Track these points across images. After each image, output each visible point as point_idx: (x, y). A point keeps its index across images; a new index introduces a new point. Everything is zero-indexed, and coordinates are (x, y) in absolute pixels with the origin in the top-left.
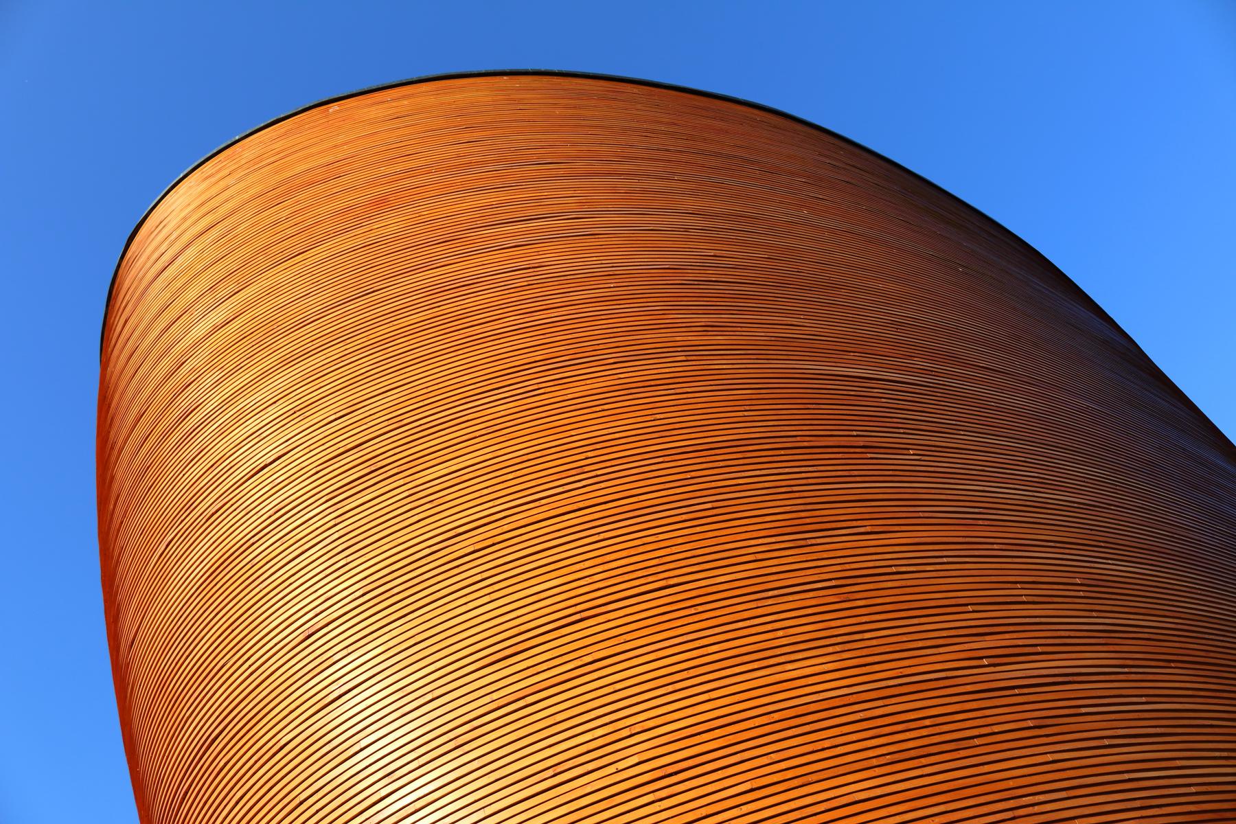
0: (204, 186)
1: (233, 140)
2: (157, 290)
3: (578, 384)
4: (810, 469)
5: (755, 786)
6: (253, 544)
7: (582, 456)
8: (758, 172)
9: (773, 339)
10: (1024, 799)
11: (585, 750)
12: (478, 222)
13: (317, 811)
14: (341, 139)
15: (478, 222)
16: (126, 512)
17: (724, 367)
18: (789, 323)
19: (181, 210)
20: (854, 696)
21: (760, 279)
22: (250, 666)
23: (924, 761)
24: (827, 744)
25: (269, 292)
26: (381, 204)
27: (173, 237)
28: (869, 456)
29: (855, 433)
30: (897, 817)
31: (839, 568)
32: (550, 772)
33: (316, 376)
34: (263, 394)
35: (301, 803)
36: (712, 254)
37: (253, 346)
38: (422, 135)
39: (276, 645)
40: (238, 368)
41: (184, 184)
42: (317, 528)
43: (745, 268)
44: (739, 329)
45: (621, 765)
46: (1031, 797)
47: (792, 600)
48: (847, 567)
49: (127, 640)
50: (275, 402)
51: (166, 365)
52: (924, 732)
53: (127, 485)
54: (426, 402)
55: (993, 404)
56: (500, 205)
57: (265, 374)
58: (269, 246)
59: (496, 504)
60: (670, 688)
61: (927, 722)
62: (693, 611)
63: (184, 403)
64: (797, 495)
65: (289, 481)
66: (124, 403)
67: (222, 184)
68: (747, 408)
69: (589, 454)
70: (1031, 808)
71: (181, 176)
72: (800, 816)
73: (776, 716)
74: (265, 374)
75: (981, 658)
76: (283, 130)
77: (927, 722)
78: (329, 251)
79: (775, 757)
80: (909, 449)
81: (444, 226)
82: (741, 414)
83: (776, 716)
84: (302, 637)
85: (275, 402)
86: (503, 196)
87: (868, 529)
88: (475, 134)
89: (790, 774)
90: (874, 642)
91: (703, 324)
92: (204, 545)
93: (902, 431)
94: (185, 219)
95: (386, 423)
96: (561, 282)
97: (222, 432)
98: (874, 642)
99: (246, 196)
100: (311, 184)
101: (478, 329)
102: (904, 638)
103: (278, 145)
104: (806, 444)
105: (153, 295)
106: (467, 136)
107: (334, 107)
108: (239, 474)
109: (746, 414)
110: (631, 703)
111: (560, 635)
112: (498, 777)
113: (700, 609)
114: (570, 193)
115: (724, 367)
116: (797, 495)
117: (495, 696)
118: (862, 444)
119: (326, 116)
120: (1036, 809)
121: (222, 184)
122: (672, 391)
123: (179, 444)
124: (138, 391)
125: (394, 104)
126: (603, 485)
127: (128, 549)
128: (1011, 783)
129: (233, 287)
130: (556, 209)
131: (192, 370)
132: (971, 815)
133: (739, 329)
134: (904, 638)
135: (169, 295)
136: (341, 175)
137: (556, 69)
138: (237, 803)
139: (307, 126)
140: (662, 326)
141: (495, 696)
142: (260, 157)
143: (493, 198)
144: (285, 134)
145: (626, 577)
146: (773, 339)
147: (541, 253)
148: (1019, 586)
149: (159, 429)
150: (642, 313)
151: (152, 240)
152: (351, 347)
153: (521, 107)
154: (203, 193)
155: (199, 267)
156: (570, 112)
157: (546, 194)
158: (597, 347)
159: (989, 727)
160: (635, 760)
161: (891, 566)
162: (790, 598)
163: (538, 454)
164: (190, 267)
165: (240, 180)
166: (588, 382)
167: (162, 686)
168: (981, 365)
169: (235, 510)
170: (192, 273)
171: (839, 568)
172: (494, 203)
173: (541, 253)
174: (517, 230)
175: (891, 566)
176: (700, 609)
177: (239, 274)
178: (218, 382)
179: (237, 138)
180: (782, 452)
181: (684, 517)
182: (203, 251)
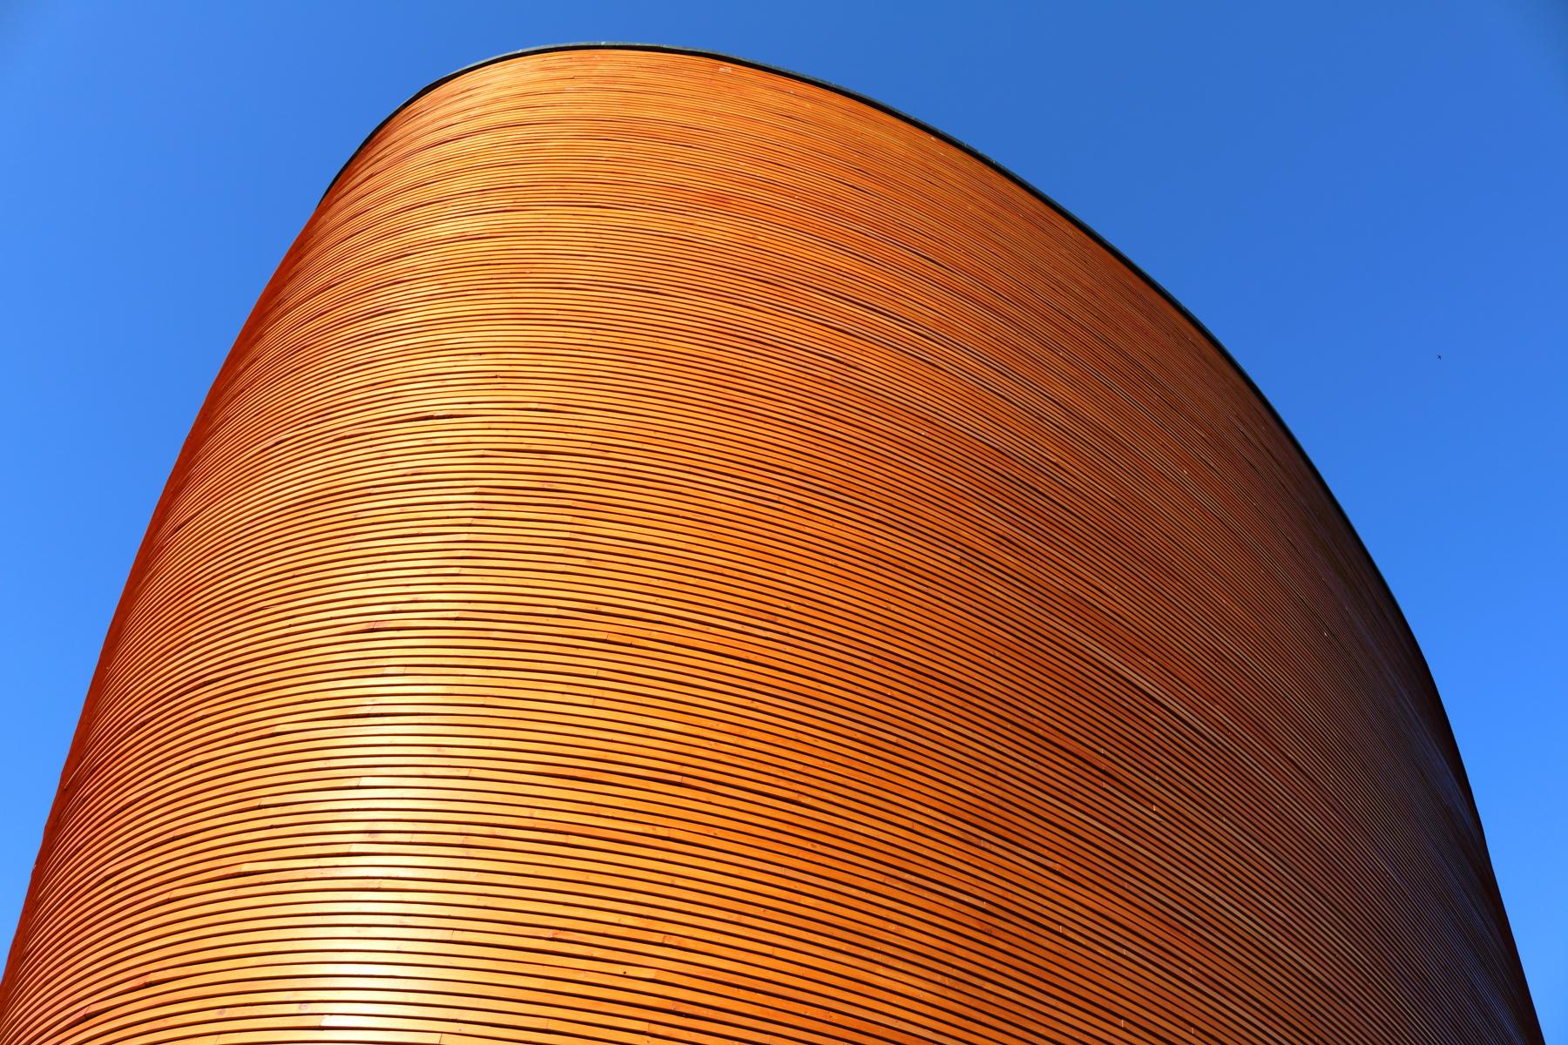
1: (598, 44)
3: (824, 521)
4: (1030, 763)
9: (1070, 593)
14: (717, 107)
19: (499, 89)
22: (290, 626)
26: (719, 201)
27: (473, 113)
28: (1105, 785)
29: (1102, 751)
32: (549, 933)
35: (260, 807)
36: (1054, 461)
38: (807, 151)
40: (462, 294)
43: (1083, 497)
45: (631, 971)
48: (1009, 896)
49: (176, 521)
50: (481, 354)
51: (386, 246)
53: (272, 354)
55: (1278, 807)
57: (489, 317)
60: (735, 917)
62: (809, 845)
63: (382, 298)
64: (998, 783)
65: (448, 448)
67: (559, 85)
68: (998, 654)
69: (793, 606)
71: (519, 52)
73: (835, 1018)
74: (489, 317)
78: (633, 222)
80: (1153, 803)
83: (835, 1018)
85: (481, 354)
86: (858, 268)
87: (1057, 867)
90: (992, 998)
91: (1001, 533)
92: (316, 465)
93: (1157, 778)
94: (497, 100)
95: (589, 445)
96: (869, 398)
97: (406, 354)
98: (992, 998)
99: (577, 112)
100: (655, 137)
103: (643, 76)
104: (1040, 732)
107: (727, 68)
109: (993, 660)
113: (819, 848)
114: (934, 305)
116: (998, 783)
117: (537, 813)
119: (712, 73)
121: (559, 85)
122: (924, 589)
124: (340, 259)
125: (795, 100)
126: (788, 649)
127: (233, 424)
129: (506, 203)
130: (908, 314)
131: (412, 269)
133: (1038, 561)
137: (994, 159)
138: (191, 767)
140: (954, 510)
141: (537, 813)
143: (845, 263)
144: (658, 67)
146: (1070, 593)
148: (1193, 1030)
149: (340, 313)
150: (938, 483)
152: (600, 339)
154: (533, 83)
155: (483, 161)
156: (986, 216)
157: (907, 291)
158: (868, 493)
161: (1059, 924)
162: (926, 894)
164: (472, 155)
165: (581, 91)
166: (837, 525)
167: (185, 592)
168: (1289, 755)
169: (371, 446)
170: (470, 163)
172: (844, 270)
173: (864, 353)
175: (1059, 924)
176: (819, 848)
178: (431, 297)
179: (603, 43)
180: (1009, 726)
181: (859, 736)
182: (497, 145)
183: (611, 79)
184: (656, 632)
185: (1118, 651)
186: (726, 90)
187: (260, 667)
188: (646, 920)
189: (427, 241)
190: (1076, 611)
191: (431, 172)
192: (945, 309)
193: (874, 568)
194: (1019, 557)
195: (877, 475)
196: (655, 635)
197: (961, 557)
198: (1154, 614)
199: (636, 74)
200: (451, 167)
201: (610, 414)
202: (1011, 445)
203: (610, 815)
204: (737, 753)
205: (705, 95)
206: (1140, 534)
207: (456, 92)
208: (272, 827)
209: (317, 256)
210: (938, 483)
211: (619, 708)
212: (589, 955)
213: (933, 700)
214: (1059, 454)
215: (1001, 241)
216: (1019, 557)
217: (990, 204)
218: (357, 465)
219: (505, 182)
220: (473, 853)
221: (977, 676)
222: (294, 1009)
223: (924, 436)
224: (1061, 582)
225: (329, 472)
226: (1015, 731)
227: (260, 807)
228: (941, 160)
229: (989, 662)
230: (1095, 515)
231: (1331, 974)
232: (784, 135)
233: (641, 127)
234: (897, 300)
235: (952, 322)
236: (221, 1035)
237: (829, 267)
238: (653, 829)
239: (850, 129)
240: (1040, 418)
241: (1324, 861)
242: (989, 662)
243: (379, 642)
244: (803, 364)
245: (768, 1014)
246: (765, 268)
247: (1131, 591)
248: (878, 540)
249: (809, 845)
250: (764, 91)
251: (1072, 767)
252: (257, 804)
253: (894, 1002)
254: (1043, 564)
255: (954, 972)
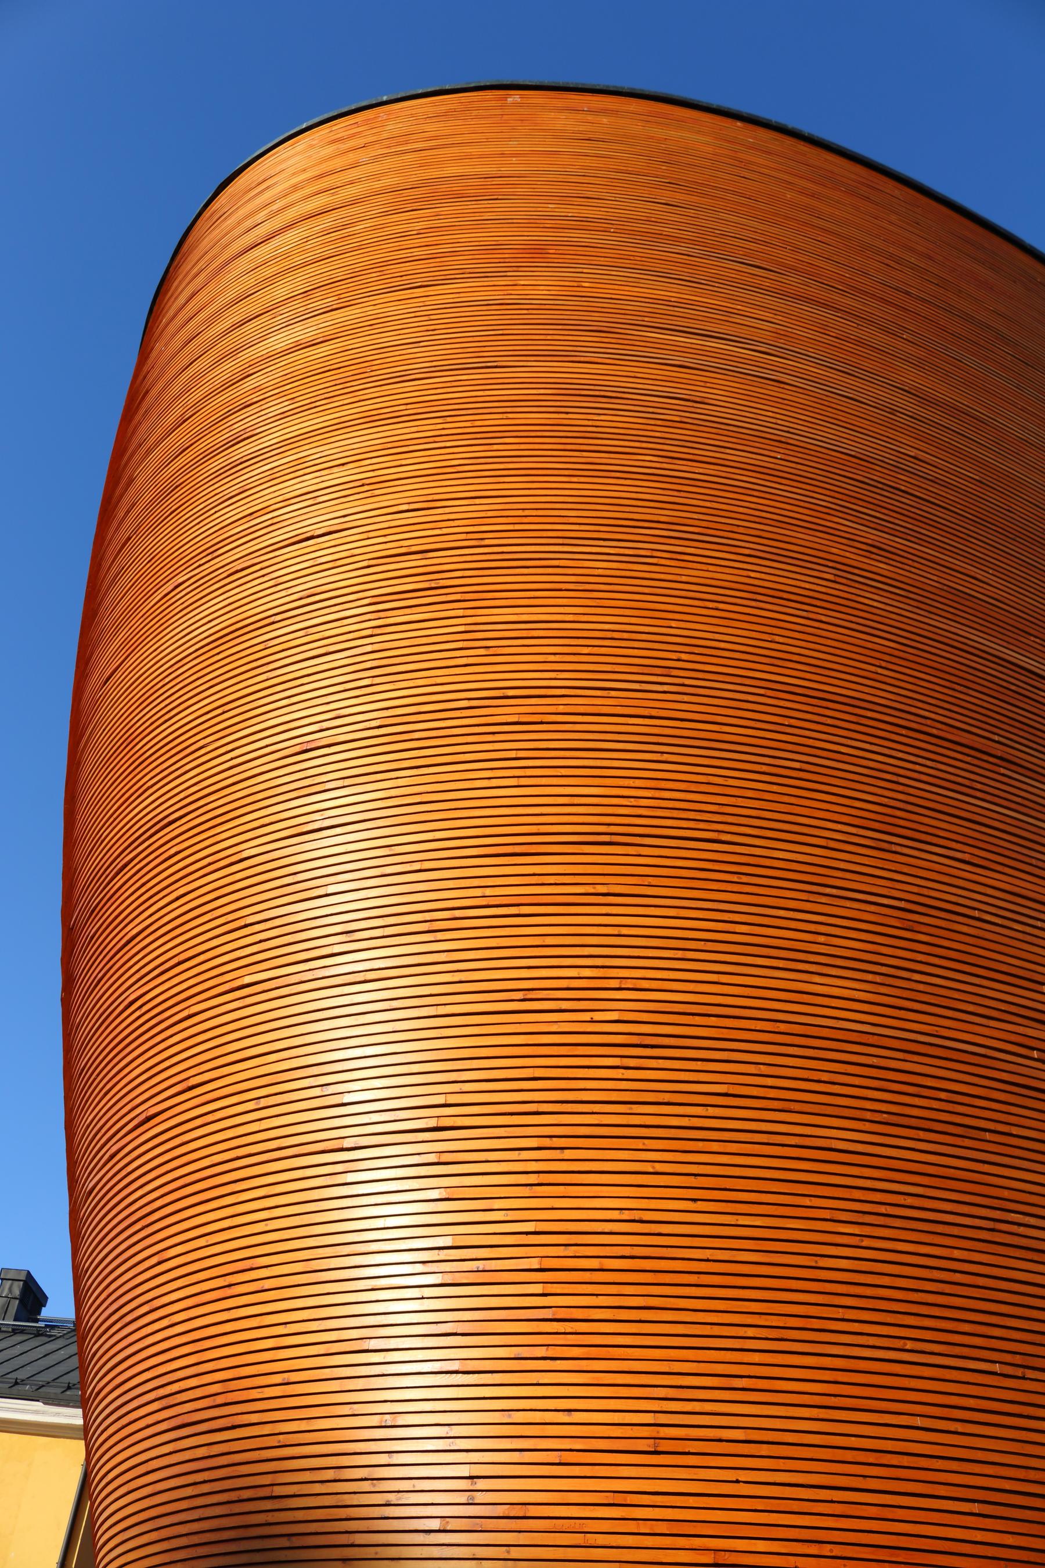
0: (330, 150)
1: (379, 100)
2: (239, 271)
3: (699, 566)
4: (929, 763)
5: (731, 1091)
6: (273, 623)
7: (674, 656)
8: (1009, 358)
9: (945, 588)
10: (1012, 1215)
11: (565, 986)
12: (646, 319)
13: (261, 941)
14: (512, 146)
15: (646, 319)
16: (139, 526)
17: (875, 604)
18: (973, 574)
19: (294, 174)
20: (876, 1037)
21: (959, 506)
22: (232, 759)
23: (922, 1135)
24: (825, 1077)
25: (373, 324)
26: (537, 252)
27: (275, 207)
28: (1003, 771)
29: (996, 738)
30: (869, 1181)
31: (915, 889)
32: (520, 995)
33: (398, 449)
34: (332, 448)
35: (246, 926)
37: (336, 385)
38: (613, 175)
39: (267, 746)
40: (311, 407)
41: (304, 139)
42: (350, 632)
43: (946, 485)
44: (910, 562)
45: (598, 1016)
46: (1021, 1216)
47: (848, 906)
48: (925, 892)
49: (102, 674)
50: (343, 464)
51: (228, 369)
52: (935, 1104)
53: (147, 497)
54: (517, 527)
56: (680, 304)
57: (341, 426)
58: (387, 263)
59: (558, 677)
60: (679, 954)
61: (943, 1095)
62: (735, 878)
63: (239, 423)
64: (901, 788)
65: (335, 564)
66: (168, 396)
67: (352, 157)
68: (884, 664)
69: (684, 656)
70: (1016, 1227)
71: (304, 126)
72: (766, 1141)
73: (782, 1027)
74: (341, 426)
75: (1033, 1049)
76: (443, 108)
77: (943, 1095)
78: (457, 295)
79: (764, 1070)
81: (603, 310)
82: (873, 668)
83: (782, 1027)
84: (297, 749)
85: (343, 464)
86: (687, 294)
87: (966, 857)
88: (678, 196)
89: (772, 1093)
90: (921, 987)
91: (869, 541)
92: (217, 602)
94: (295, 188)
95: (463, 536)
96: (721, 432)
97: (272, 478)
98: (921, 987)
99: (377, 185)
100: (460, 196)
101: (604, 458)
102: (956, 995)
103: (432, 128)
104: (935, 732)
105: (234, 273)
106: (666, 196)
107: (515, 97)
108: (280, 535)
109: (879, 670)
110: (632, 954)
111: (581, 852)
112: (463, 979)
113: (745, 879)
114: (768, 316)
115: (875, 604)
116: (901, 788)
117: (488, 892)
118: (999, 754)
119: (502, 107)
120: (1022, 1230)
121: (352, 157)
122: (804, 614)
123: (219, 474)
124: (187, 390)
125: (590, 118)
126: (686, 698)
127: (130, 573)
128: (1006, 1194)
129: (330, 301)
130: (744, 332)
131: (257, 389)
132: (948, 1209)
133: (910, 562)
134: (956, 995)
135: (252, 282)
136: (500, 197)
137: (807, 129)
138: (177, 899)
139: (475, 113)
140: (821, 528)
141: (488, 892)
142: (405, 138)
143: (672, 292)
144: (446, 114)
145: (675, 814)
146: (945, 588)
147: (708, 385)
149: (201, 446)
150: (802, 504)
151: (249, 200)
152: (451, 427)
153: (747, 175)
154: (326, 160)
155: (298, 260)
156: (806, 200)
157: (739, 307)
158: (735, 529)
159: (1009, 1126)
160: (614, 1016)
161: (974, 909)
162: (848, 904)
163: (625, 636)
164: (287, 255)
165: (375, 160)
166: (711, 568)
167: (129, 741)
169: (263, 576)
170: (286, 264)
171: (915, 889)
172: (673, 299)
173: (708, 385)
174: (689, 346)
175: (974, 909)
176: (745, 879)
177: (343, 286)
178: (284, 416)
179: (385, 98)
180: (904, 732)
181: (764, 768)
182: (307, 240)
183: (402, 139)
184: (561, 705)
185: (1001, 636)
186: (519, 123)
187: (216, 801)
188: (601, 969)
189: (265, 357)
190: (955, 605)
191: (250, 281)
192: (780, 318)
193: (754, 604)
194: (891, 562)
195: (741, 510)
196: (561, 709)
197: (835, 575)
198: (1032, 590)
199: (426, 128)
200: (269, 272)
201: (477, 501)
202: (865, 447)
203: (552, 882)
204: (656, 805)
205: (499, 135)
206: (1008, 511)
207: (253, 185)
208: (261, 941)
209: (164, 389)
210: (802, 504)
211: (543, 783)
212: (558, 1008)
213: (829, 721)
214: (916, 446)
215: (827, 225)
216: (891, 562)
217: (809, 185)
218: (255, 597)
219: (323, 279)
220: (440, 936)
221: (866, 690)
222: (317, 1092)
223: (781, 459)
224: (935, 578)
225: (231, 607)
226: (892, 713)
227: (246, 926)
228: (750, 148)
229: (877, 673)
230: (961, 502)
231: (936, 409)
232: (587, 162)
233: (443, 188)
234: (730, 319)
235: (790, 330)
236: (262, 1121)
237: (656, 301)
238: (594, 888)
239: (652, 138)
240: (893, 412)
241: (986, 369)
242: (877, 673)
243: (314, 762)
244: (651, 410)
245: (722, 1033)
246: (596, 316)
247: (1006, 572)
248: (752, 574)
249: (735, 878)
250: (558, 115)
251: (968, 759)
252: (243, 924)
253: (833, 1005)
254: (916, 565)
255: (884, 970)
